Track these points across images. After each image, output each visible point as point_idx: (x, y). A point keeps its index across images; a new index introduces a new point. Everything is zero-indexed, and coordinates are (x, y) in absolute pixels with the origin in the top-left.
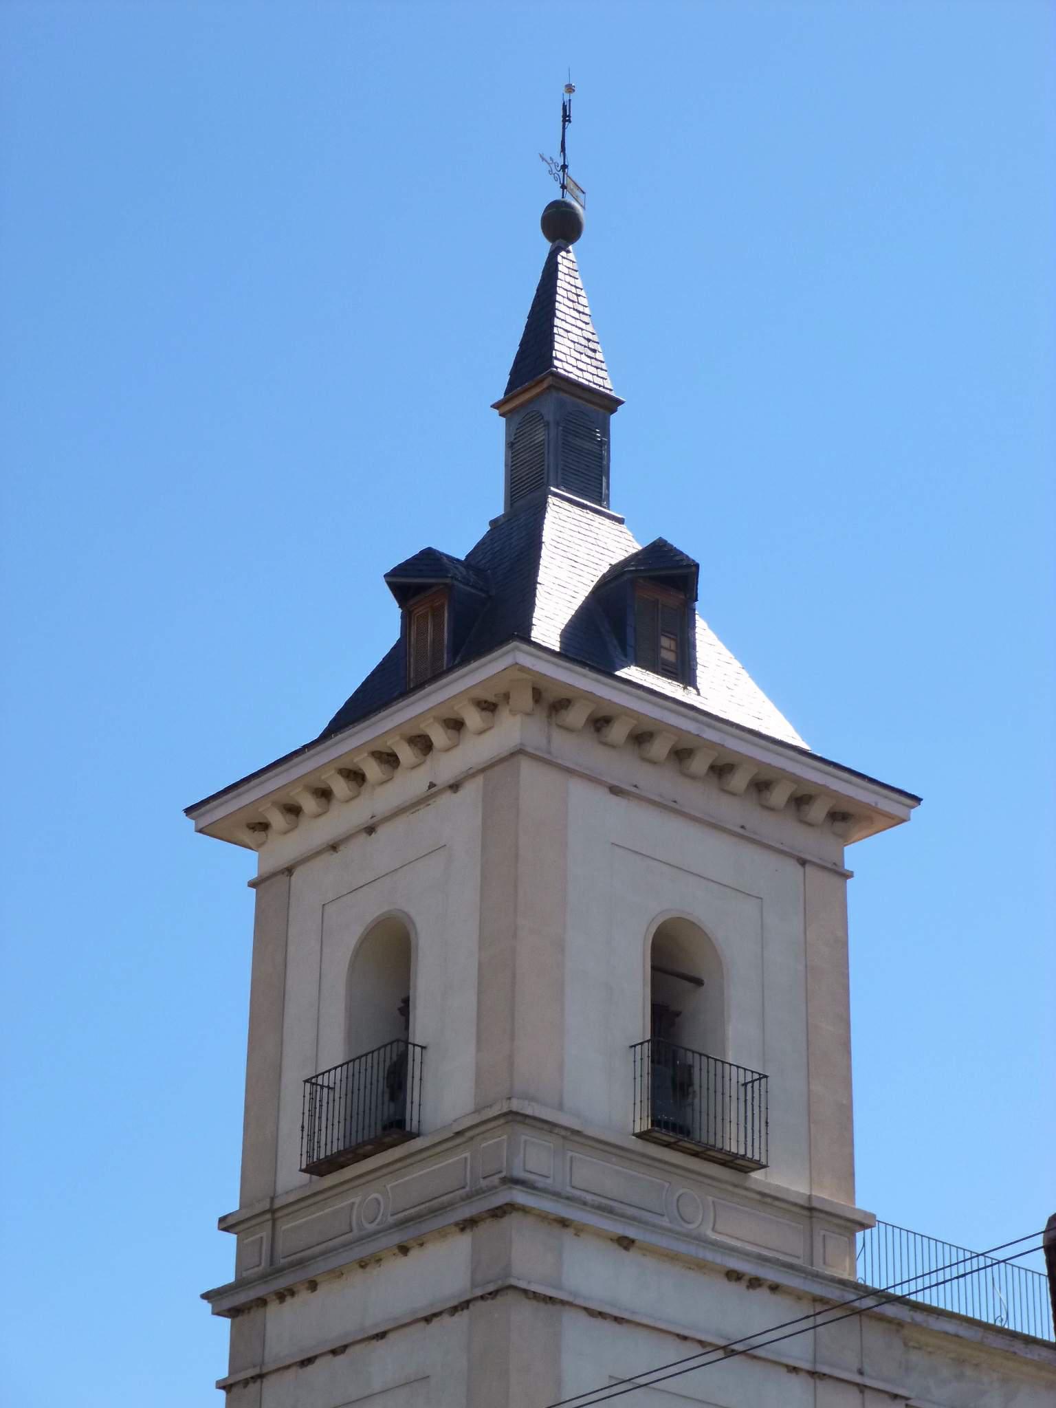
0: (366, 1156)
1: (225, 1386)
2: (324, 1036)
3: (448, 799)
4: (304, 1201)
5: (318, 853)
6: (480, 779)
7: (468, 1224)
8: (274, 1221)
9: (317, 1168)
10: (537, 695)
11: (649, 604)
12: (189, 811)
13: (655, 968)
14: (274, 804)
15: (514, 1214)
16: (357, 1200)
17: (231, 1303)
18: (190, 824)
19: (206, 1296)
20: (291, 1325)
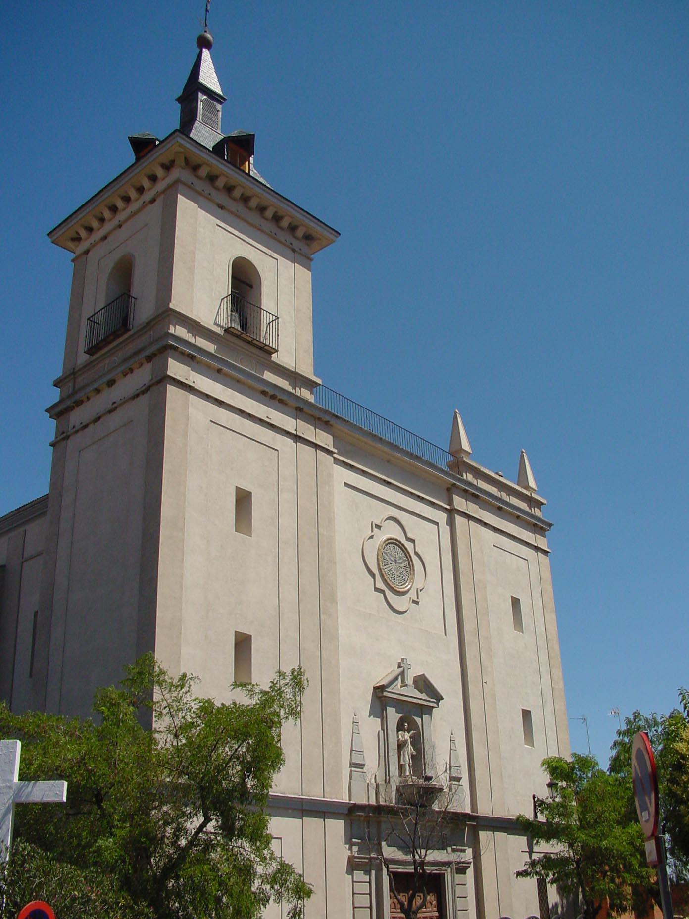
0: (110, 343)
1: (53, 445)
2: (97, 299)
3: (150, 208)
4: (88, 366)
5: (128, 400)
6: (162, 196)
7: (149, 359)
8: (75, 378)
9: (90, 351)
10: (187, 161)
11: (238, 147)
12: (48, 235)
13: (234, 277)
14: (82, 225)
15: (134, 161)
16: (107, 362)
17: (58, 412)
18: (49, 240)
19: (47, 411)
20: (77, 417)
